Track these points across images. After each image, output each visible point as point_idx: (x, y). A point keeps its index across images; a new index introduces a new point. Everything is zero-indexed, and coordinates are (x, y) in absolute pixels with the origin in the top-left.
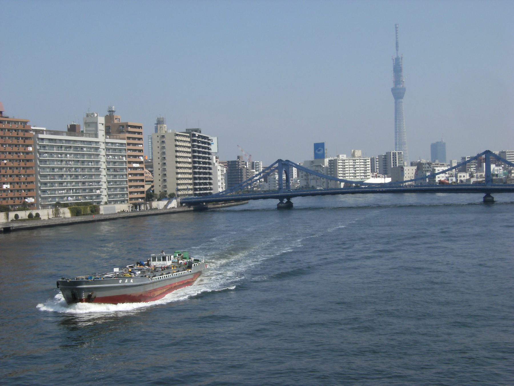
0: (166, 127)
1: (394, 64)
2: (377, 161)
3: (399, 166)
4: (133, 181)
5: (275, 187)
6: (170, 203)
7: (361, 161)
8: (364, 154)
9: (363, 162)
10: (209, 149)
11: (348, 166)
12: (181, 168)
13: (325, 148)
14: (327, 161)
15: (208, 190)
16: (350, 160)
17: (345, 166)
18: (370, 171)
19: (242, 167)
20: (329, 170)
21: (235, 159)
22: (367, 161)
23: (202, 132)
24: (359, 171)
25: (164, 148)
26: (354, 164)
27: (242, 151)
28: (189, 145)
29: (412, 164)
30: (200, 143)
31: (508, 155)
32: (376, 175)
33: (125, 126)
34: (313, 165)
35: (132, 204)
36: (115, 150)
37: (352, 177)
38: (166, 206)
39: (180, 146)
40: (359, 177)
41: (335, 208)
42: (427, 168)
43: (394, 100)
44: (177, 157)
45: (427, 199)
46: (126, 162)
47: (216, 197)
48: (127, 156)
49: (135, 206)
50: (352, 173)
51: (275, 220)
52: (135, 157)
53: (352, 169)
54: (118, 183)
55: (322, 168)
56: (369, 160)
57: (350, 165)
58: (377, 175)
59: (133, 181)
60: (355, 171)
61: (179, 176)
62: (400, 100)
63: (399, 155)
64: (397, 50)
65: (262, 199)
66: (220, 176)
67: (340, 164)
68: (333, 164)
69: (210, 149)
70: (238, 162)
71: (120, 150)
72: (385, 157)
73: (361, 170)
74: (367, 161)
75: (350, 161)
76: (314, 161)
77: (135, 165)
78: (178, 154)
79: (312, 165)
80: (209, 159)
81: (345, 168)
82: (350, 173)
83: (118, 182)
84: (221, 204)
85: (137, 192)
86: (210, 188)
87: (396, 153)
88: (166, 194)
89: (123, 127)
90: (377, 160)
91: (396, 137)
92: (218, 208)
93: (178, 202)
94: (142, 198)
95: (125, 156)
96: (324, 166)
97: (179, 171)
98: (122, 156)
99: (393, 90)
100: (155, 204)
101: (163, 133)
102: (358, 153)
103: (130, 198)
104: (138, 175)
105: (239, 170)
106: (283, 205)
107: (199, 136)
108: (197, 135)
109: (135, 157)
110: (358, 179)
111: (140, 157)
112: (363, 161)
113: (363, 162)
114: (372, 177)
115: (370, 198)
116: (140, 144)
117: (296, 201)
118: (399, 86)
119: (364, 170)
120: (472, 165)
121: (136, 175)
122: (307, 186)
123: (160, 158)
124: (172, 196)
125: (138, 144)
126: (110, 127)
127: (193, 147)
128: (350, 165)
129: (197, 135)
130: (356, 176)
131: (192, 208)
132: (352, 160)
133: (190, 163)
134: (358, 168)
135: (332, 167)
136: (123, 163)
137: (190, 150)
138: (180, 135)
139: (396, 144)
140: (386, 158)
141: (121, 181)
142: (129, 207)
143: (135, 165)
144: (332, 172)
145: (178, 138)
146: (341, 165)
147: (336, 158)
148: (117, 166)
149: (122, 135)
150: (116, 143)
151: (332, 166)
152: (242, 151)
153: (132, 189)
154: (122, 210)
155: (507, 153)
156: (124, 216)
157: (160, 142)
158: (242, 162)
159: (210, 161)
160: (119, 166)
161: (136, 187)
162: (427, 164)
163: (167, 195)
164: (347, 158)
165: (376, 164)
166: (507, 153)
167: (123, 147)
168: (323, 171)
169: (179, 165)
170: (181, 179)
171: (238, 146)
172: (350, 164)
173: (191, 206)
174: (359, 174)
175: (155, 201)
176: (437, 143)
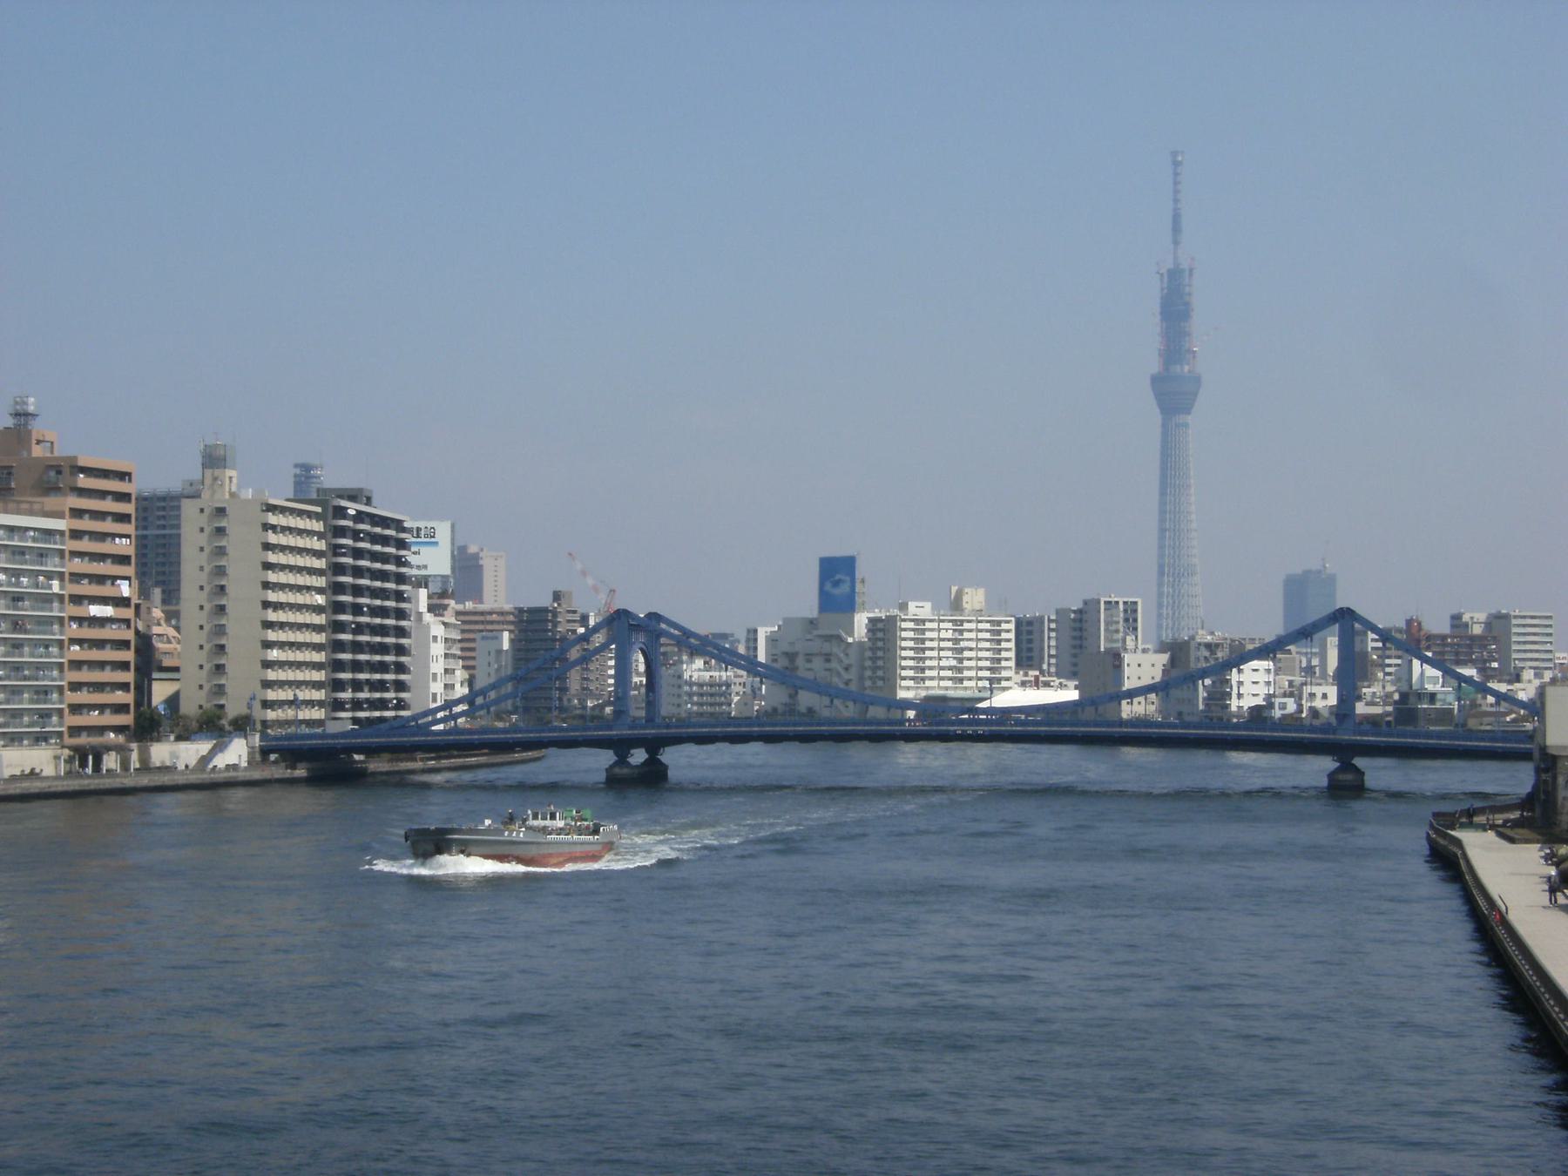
0: (234, 480)
1: (1162, 289)
2: (1053, 630)
3: (1108, 651)
4: (85, 667)
5: (679, 705)
6: (222, 750)
7: (981, 626)
8: (996, 602)
9: (987, 631)
10: (400, 561)
11: (935, 644)
12: (282, 625)
13: (858, 576)
14: (861, 620)
15: (387, 709)
16: (943, 621)
17: (923, 641)
18: (1012, 664)
19: (568, 630)
20: (868, 654)
21: (545, 601)
22: (1004, 626)
23: (374, 501)
24: (972, 663)
25: (221, 552)
26: (957, 635)
27: (584, 573)
28: (320, 545)
29: (1162, 648)
30: (362, 540)
31: (1519, 626)
32: (1037, 678)
33: (66, 471)
34: (815, 633)
35: (70, 748)
36: (23, 554)
37: (950, 684)
38: (205, 760)
39: (283, 549)
40: (972, 684)
41: (829, 789)
42: (1202, 659)
43: (1160, 417)
44: (266, 585)
45: (1198, 769)
46: (61, 598)
47: (388, 736)
48: (67, 576)
49: (81, 754)
50: (950, 668)
51: (1320, 832)
52: (100, 579)
53: (949, 654)
54: (26, 672)
55: (843, 646)
56: (1012, 626)
57: (943, 640)
58: (1042, 679)
59: (85, 667)
60: (961, 660)
61: (274, 654)
62: (1181, 418)
63: (1109, 612)
64: (1176, 243)
65: (797, 743)
66: (441, 660)
67: (906, 633)
68: (883, 631)
69: (406, 564)
70: (555, 613)
71: (41, 555)
72: (1079, 616)
73: (980, 659)
74: (1004, 626)
75: (942, 625)
76: (816, 619)
77: (96, 610)
78: (272, 577)
79: (810, 633)
80: (399, 596)
81: (923, 650)
82: (943, 668)
83: (26, 666)
84: (422, 760)
85: (102, 708)
86: (400, 700)
87: (1117, 603)
88: (220, 718)
89: (59, 472)
90: (1053, 626)
91: (1161, 547)
92: (412, 772)
93: (253, 748)
94: (118, 729)
95: (61, 576)
96: (850, 640)
97: (272, 636)
98: (50, 576)
99: (1156, 381)
100: (161, 752)
101: (222, 498)
102: (974, 598)
103: (70, 728)
104: (108, 646)
105: (555, 640)
106: (626, 771)
107: (360, 517)
108: (351, 512)
109: (100, 579)
110: (968, 689)
111: (119, 582)
112: (987, 626)
113: (987, 631)
114: (1023, 684)
115: (977, 760)
116: (121, 536)
117: (680, 760)
118: (1178, 367)
119: (992, 660)
120: (1389, 657)
121: (100, 644)
122: (791, 709)
123: (207, 589)
124: (242, 725)
125: (114, 536)
126: (14, 471)
127: (336, 554)
128: (943, 640)
129: (351, 512)
130: (923, 679)
131: (301, 772)
132: (950, 621)
133: (318, 609)
134: (971, 649)
135: (880, 644)
136: (52, 602)
137: (320, 564)
138: (283, 510)
139: (1161, 573)
140: (1081, 621)
141: (39, 667)
142: (57, 758)
143: (96, 610)
144: (880, 663)
145: (273, 519)
146: (911, 639)
147: (896, 612)
148: (27, 610)
149: (51, 502)
150: (27, 529)
151: (880, 640)
152: (584, 573)
153: (83, 697)
154: (27, 771)
155: (1514, 622)
156: (25, 792)
157: (207, 530)
158: (569, 612)
159: (403, 605)
160: (34, 610)
161: (99, 687)
162: (1202, 648)
163: (224, 722)
164: (934, 615)
165: (1049, 638)
166: (1514, 622)
167: (55, 543)
168: (847, 655)
169: (272, 616)
170: (281, 664)
171: (570, 554)
172: (943, 635)
173: (299, 765)
174: (972, 673)
175: (168, 741)
176: (1307, 573)
